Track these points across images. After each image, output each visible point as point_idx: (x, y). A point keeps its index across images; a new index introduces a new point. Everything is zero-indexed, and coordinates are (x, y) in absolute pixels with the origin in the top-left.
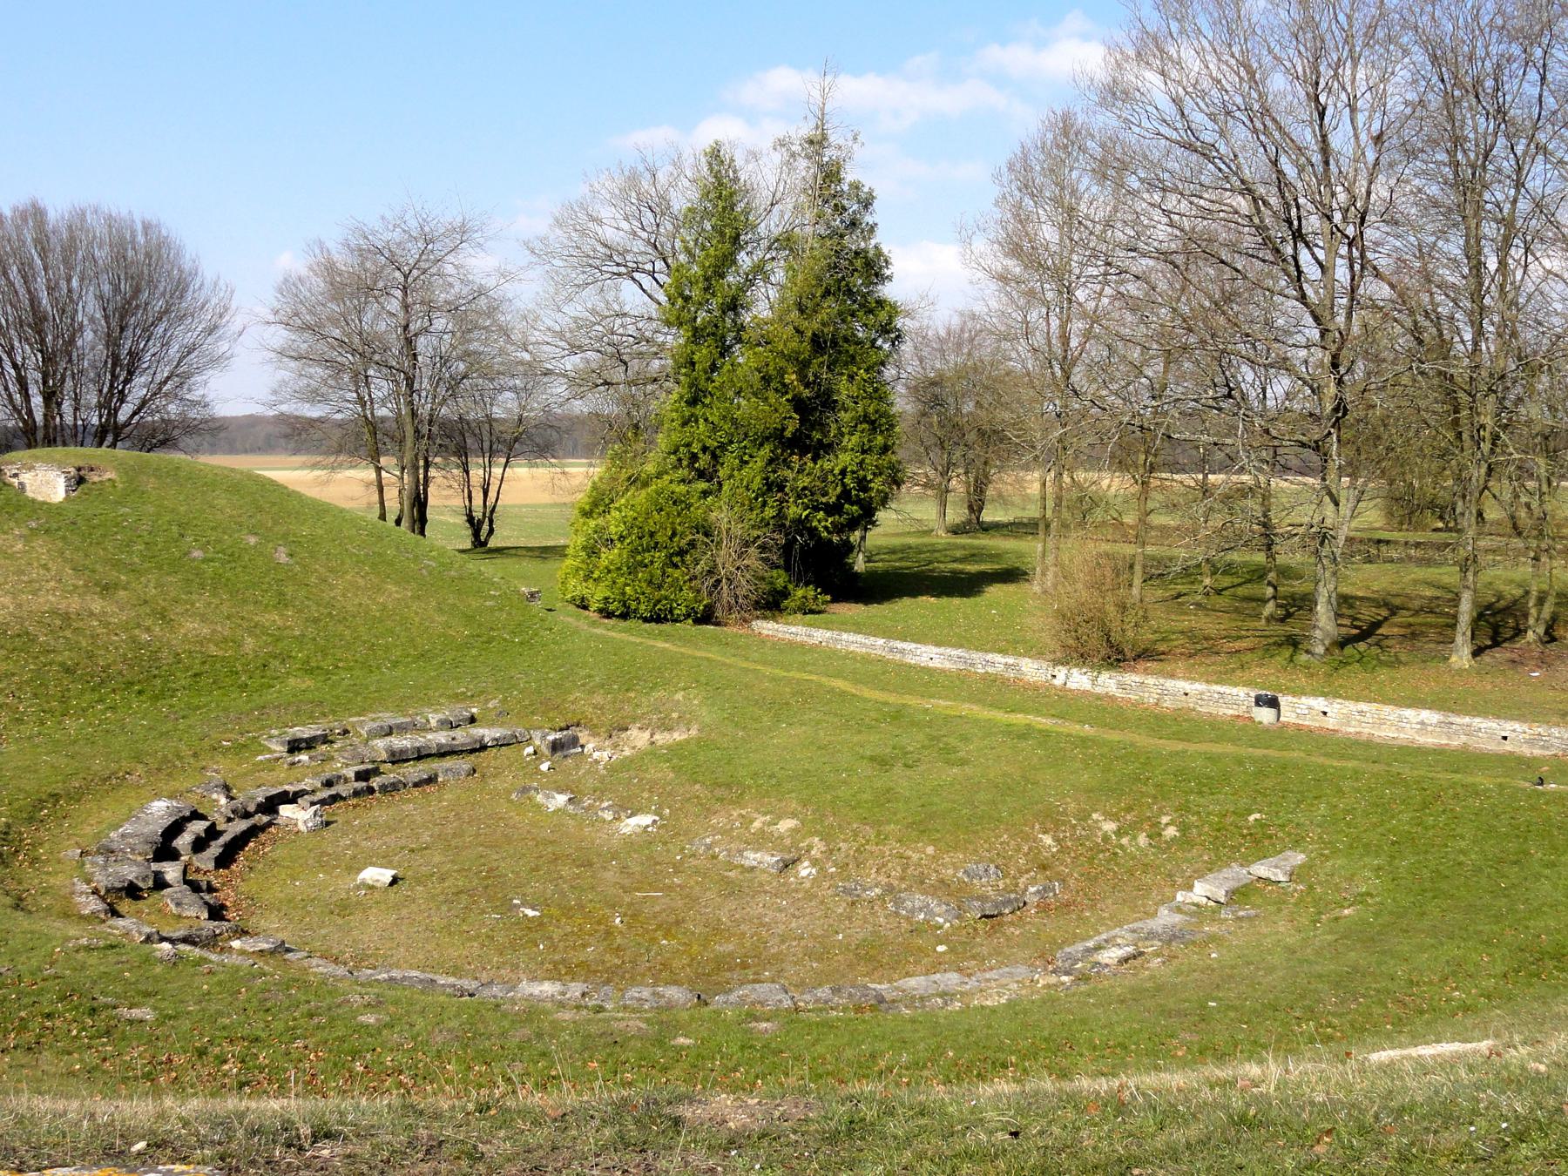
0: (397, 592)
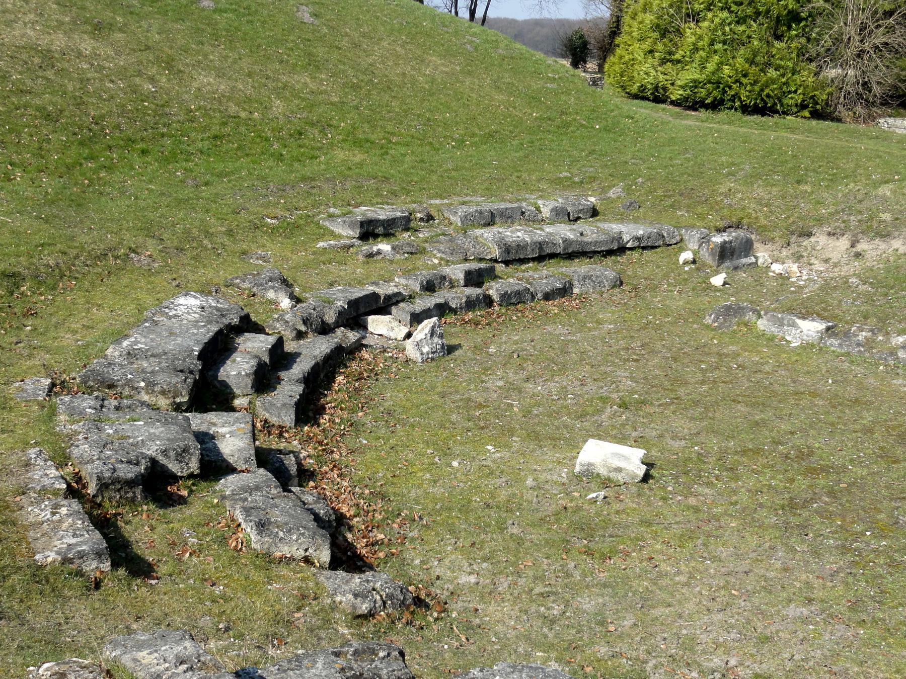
0: (443, 64)
